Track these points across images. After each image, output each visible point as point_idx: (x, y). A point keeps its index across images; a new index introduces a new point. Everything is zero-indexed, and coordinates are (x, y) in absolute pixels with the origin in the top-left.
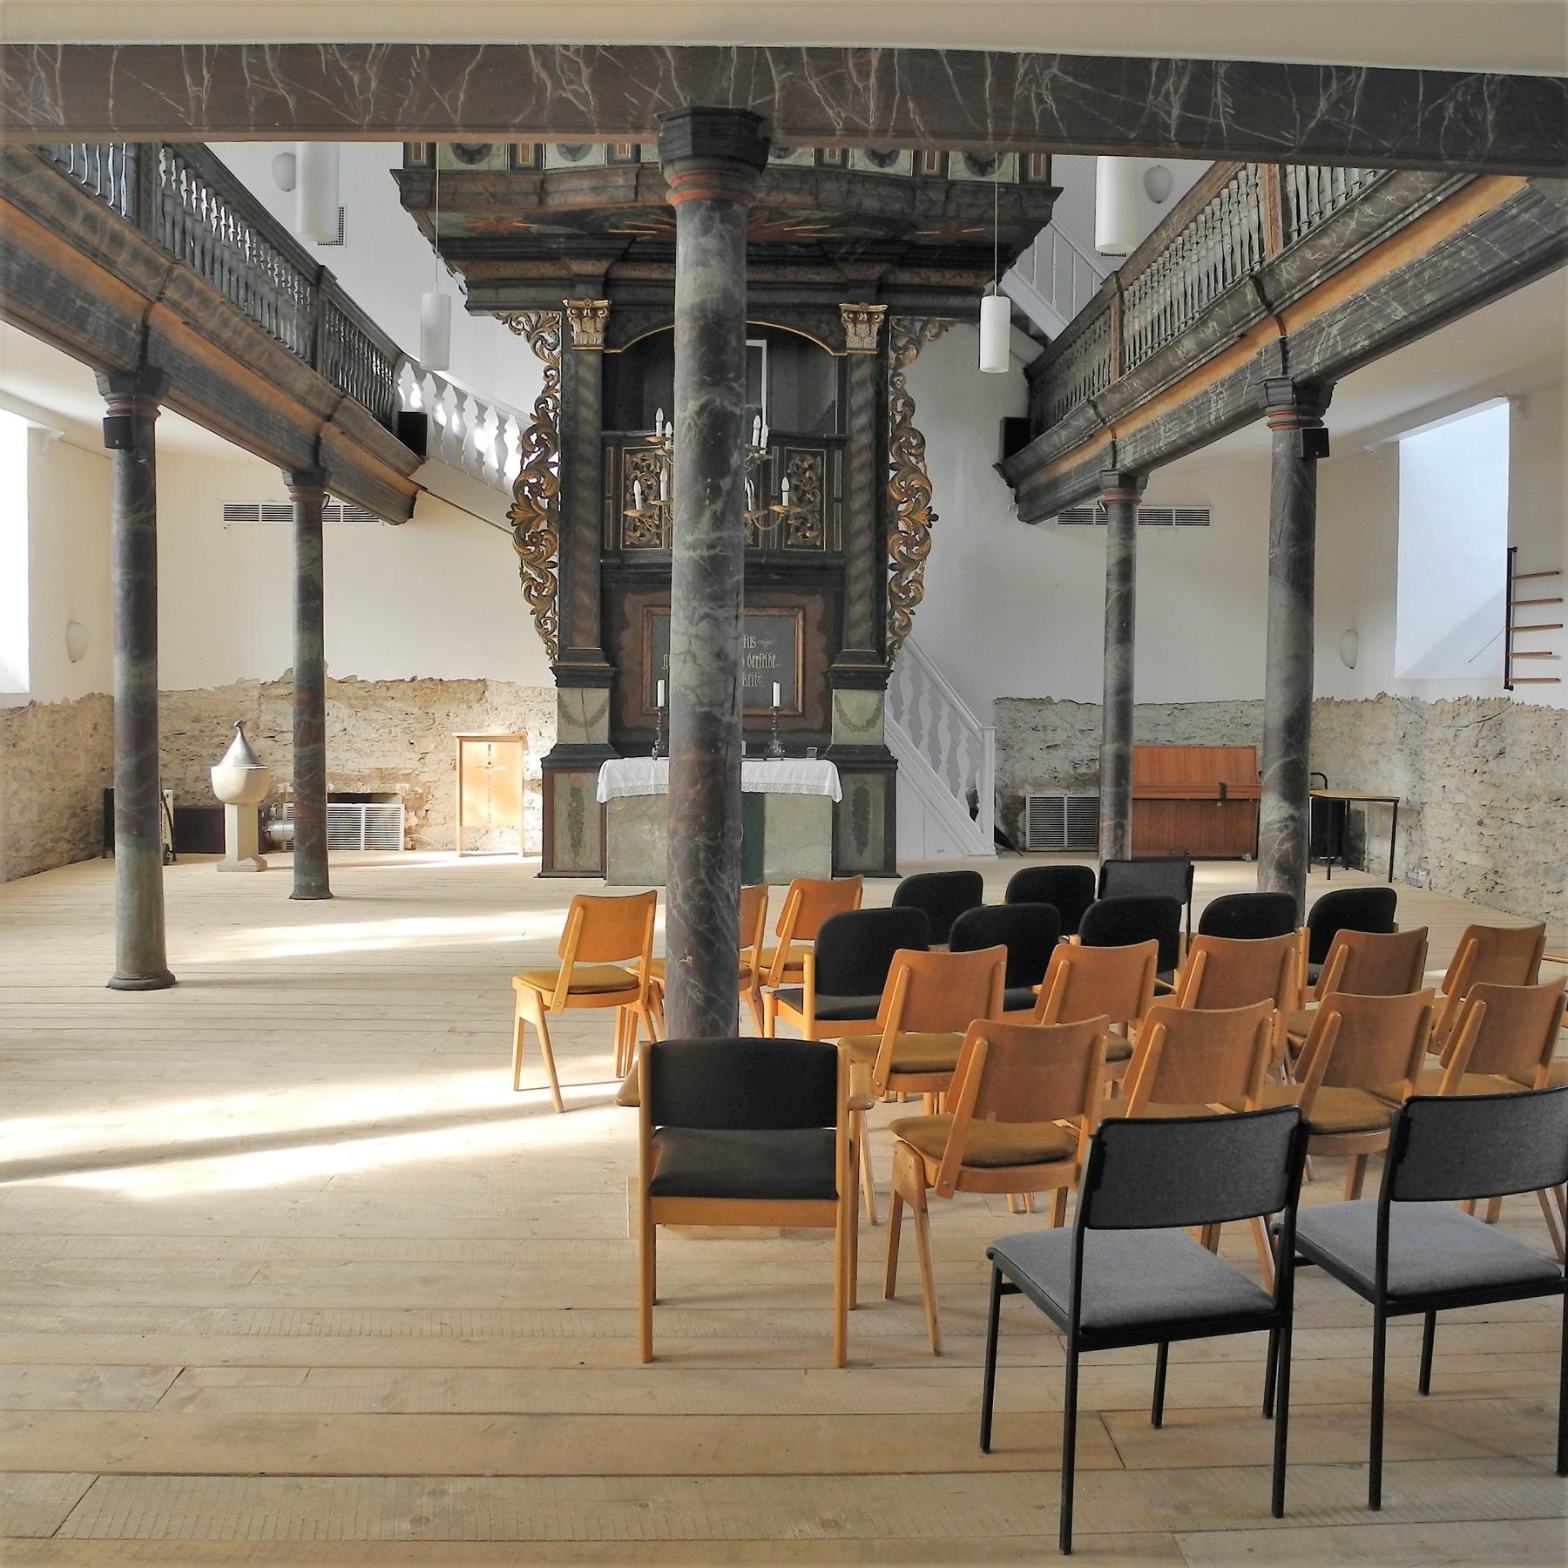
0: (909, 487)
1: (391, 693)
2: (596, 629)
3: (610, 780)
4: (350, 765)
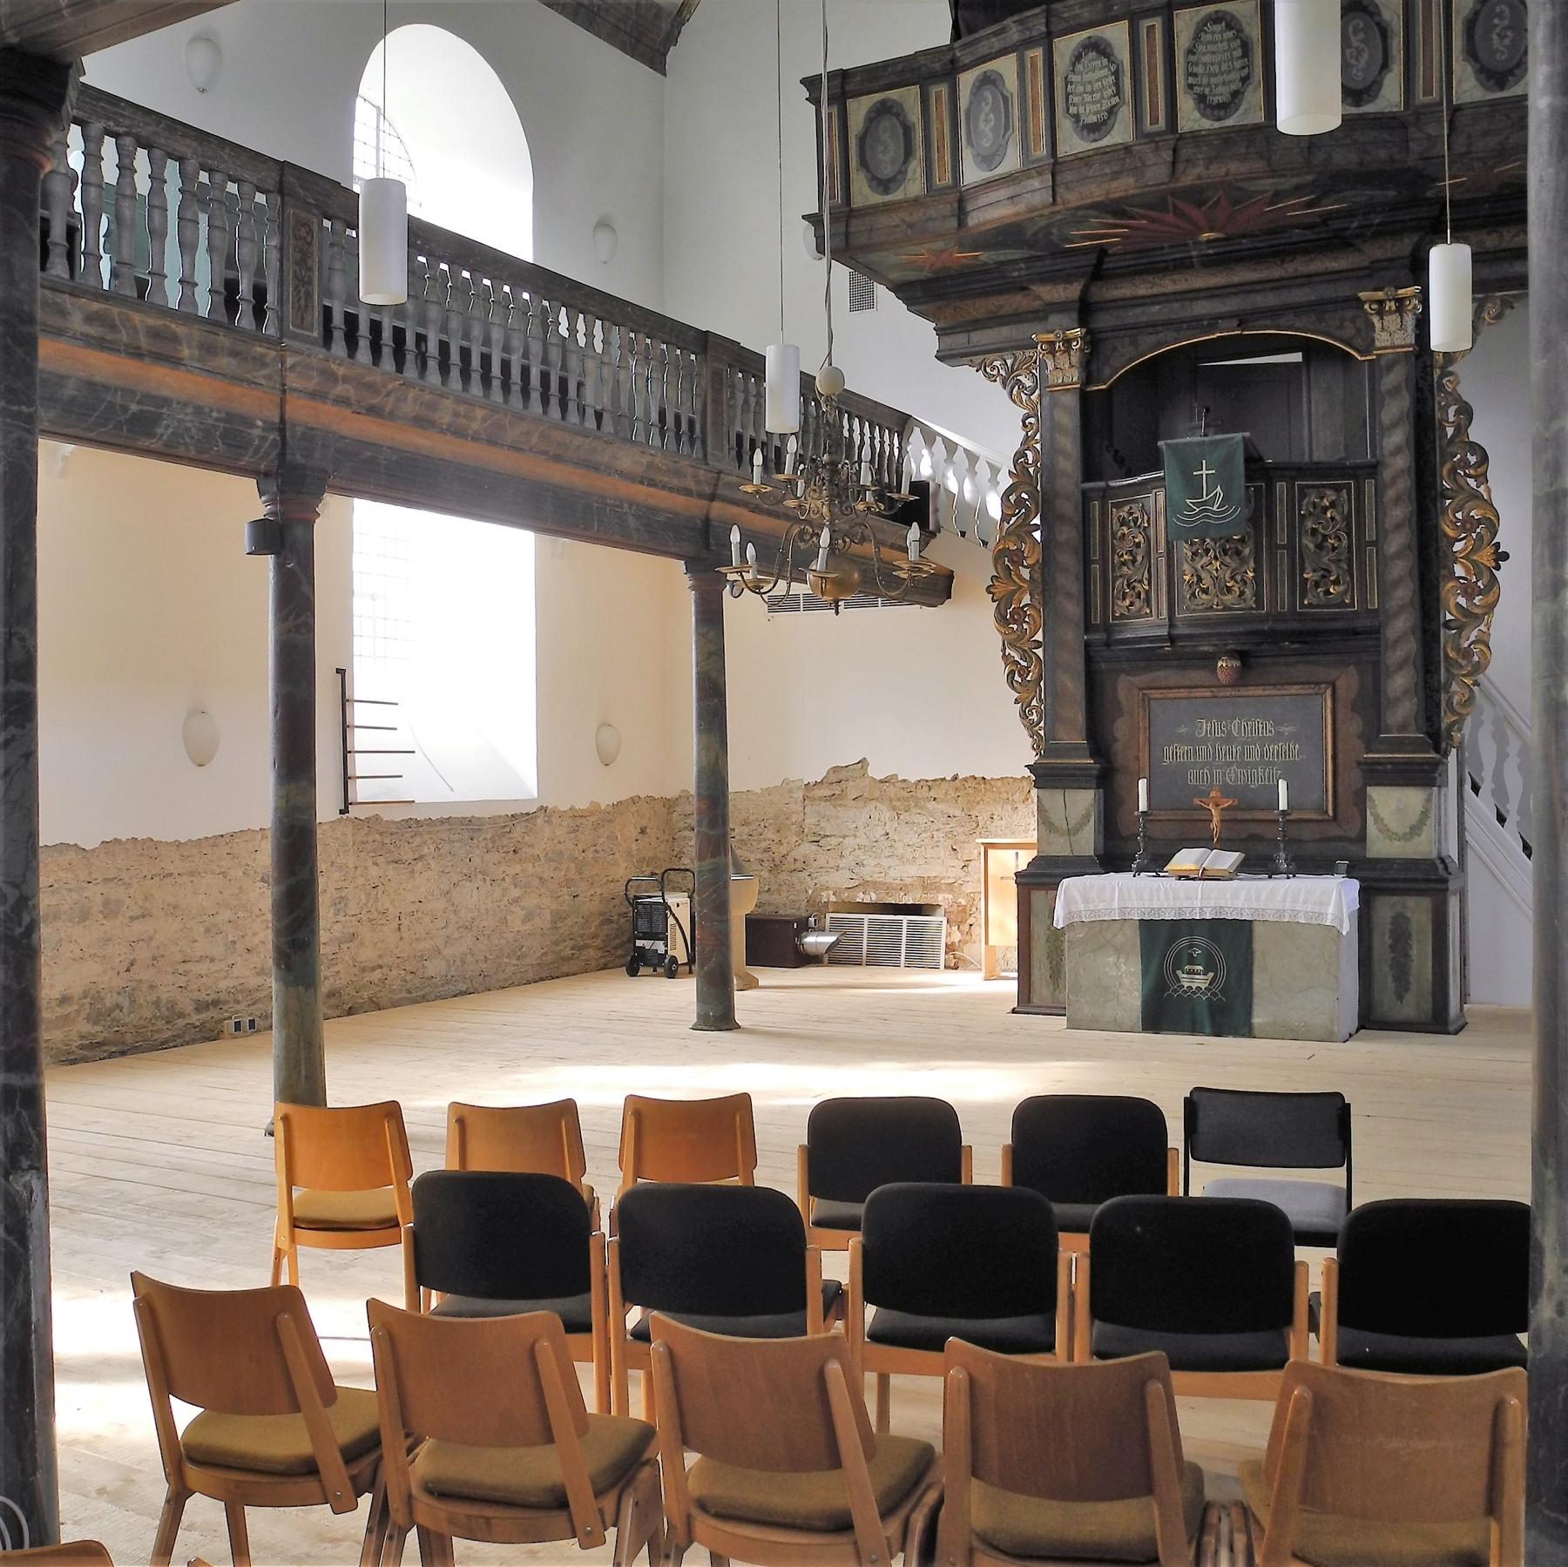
0: (1468, 519)
1: (932, 793)
2: (1080, 718)
3: (1067, 902)
4: (892, 873)
